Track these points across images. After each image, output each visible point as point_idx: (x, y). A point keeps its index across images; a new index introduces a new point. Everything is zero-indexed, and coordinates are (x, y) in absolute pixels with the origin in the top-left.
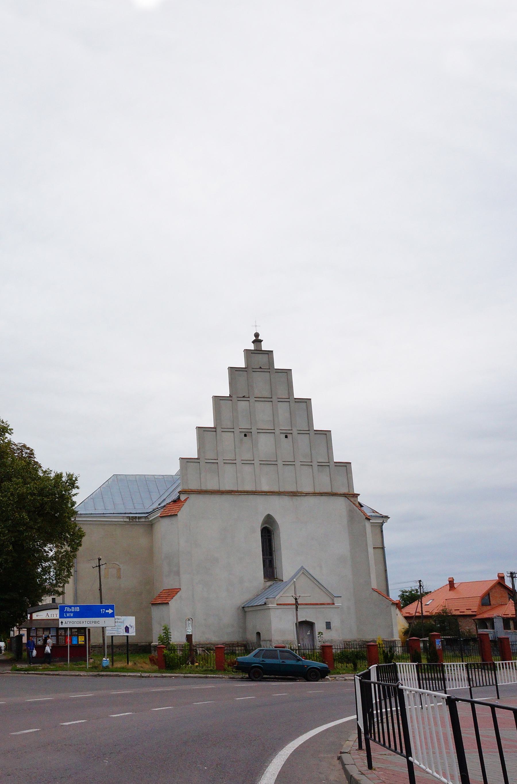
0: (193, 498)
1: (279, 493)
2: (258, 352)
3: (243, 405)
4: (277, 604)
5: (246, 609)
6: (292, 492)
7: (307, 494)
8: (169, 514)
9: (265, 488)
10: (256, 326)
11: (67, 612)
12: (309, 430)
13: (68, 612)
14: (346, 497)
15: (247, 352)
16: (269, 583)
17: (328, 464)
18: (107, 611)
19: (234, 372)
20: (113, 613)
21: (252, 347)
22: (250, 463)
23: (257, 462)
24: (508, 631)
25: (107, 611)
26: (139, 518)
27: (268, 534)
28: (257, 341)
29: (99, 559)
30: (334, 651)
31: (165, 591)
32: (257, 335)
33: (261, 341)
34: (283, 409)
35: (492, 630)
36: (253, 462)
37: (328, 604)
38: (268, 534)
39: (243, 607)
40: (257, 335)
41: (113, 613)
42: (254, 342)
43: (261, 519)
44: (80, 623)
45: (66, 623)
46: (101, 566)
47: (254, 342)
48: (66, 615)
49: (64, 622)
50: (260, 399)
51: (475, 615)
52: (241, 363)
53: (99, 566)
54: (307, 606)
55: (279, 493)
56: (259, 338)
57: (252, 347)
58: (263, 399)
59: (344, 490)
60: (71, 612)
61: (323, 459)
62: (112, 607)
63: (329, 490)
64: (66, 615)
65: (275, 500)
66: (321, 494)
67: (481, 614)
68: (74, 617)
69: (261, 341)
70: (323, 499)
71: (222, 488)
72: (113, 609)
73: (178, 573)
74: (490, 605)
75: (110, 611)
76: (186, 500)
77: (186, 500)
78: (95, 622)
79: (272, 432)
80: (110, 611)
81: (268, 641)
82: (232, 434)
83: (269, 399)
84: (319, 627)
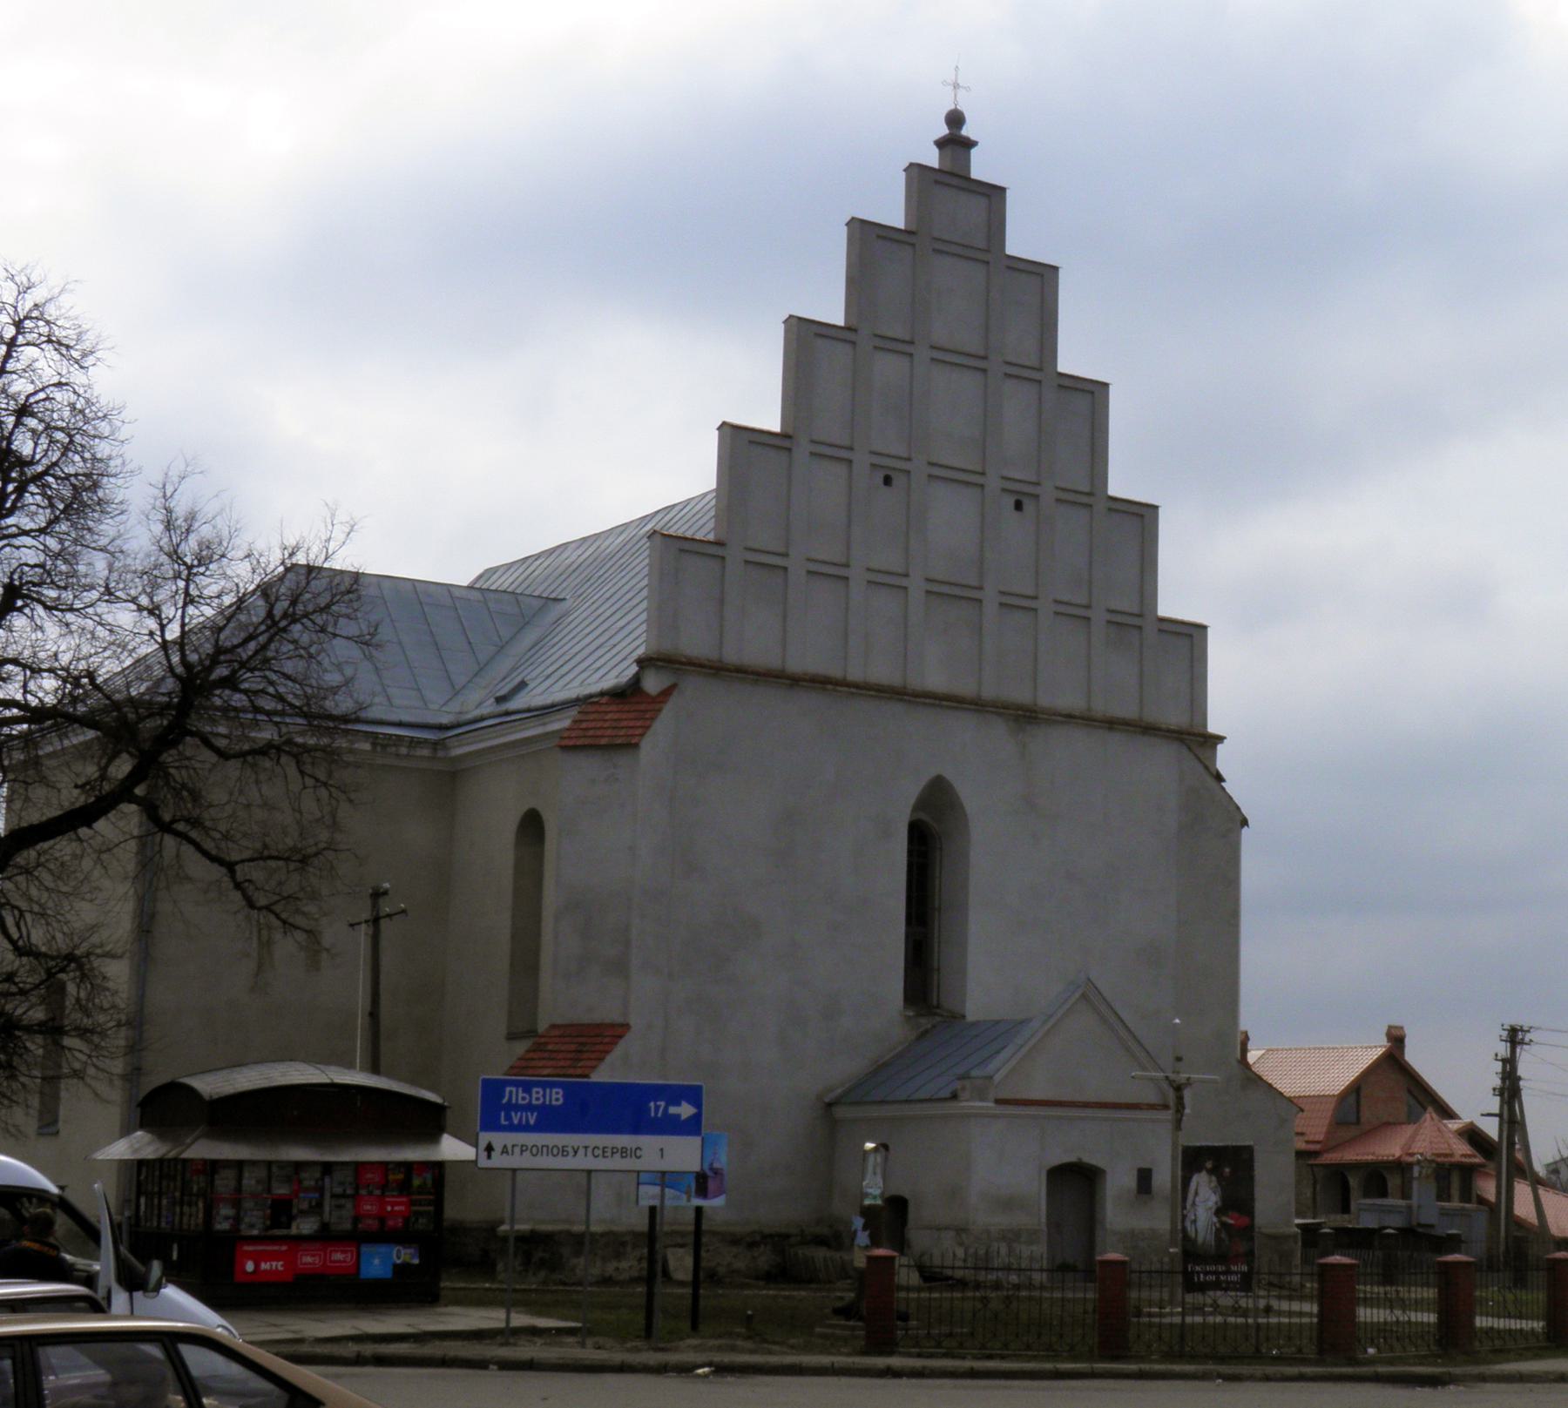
0: (693, 689)
1: (976, 705)
2: (955, 181)
3: (888, 368)
4: (998, 1102)
5: (841, 1112)
6: (1019, 707)
7: (1069, 718)
8: (603, 741)
9: (935, 679)
10: (956, 86)
11: (512, 1107)
12: (1089, 494)
13: (517, 1108)
14: (1182, 741)
15: (916, 172)
16: (925, 1023)
17: (1137, 621)
18: (673, 1110)
19: (866, 238)
20: (697, 1118)
21: (932, 158)
22: (889, 582)
23: (916, 586)
24: (1379, 1201)
25: (673, 1110)
26: (414, 743)
27: (929, 844)
28: (956, 143)
29: (377, 895)
30: (1362, 1287)
31: (557, 1033)
32: (955, 119)
33: (969, 144)
34: (1016, 404)
35: (1401, 1202)
36: (904, 582)
37: (1152, 1107)
38: (929, 844)
39: (830, 1105)
40: (955, 119)
41: (697, 1118)
42: (941, 144)
43: (908, 792)
44: (563, 1151)
45: (505, 1151)
46: (384, 923)
47: (941, 144)
48: (508, 1118)
49: (498, 1147)
50: (946, 357)
51: (1315, 1154)
52: (892, 212)
53: (376, 921)
54: (1089, 1112)
55: (976, 705)
56: (965, 132)
57: (932, 158)
58: (964, 360)
59: (1174, 717)
60: (529, 1107)
61: (1127, 603)
62: (693, 1094)
63: (1128, 711)
64: (508, 1118)
65: (963, 727)
66: (1112, 724)
67: (1327, 1151)
68: (539, 1128)
69: (969, 144)
70: (1116, 740)
71: (795, 666)
72: (697, 1104)
73: (619, 967)
74: (1358, 1122)
75: (685, 1110)
76: (666, 693)
77: (666, 693)
78: (624, 1152)
79: (970, 480)
80: (685, 1110)
81: (947, 1228)
82: (841, 470)
83: (976, 362)
84: (1119, 1181)
